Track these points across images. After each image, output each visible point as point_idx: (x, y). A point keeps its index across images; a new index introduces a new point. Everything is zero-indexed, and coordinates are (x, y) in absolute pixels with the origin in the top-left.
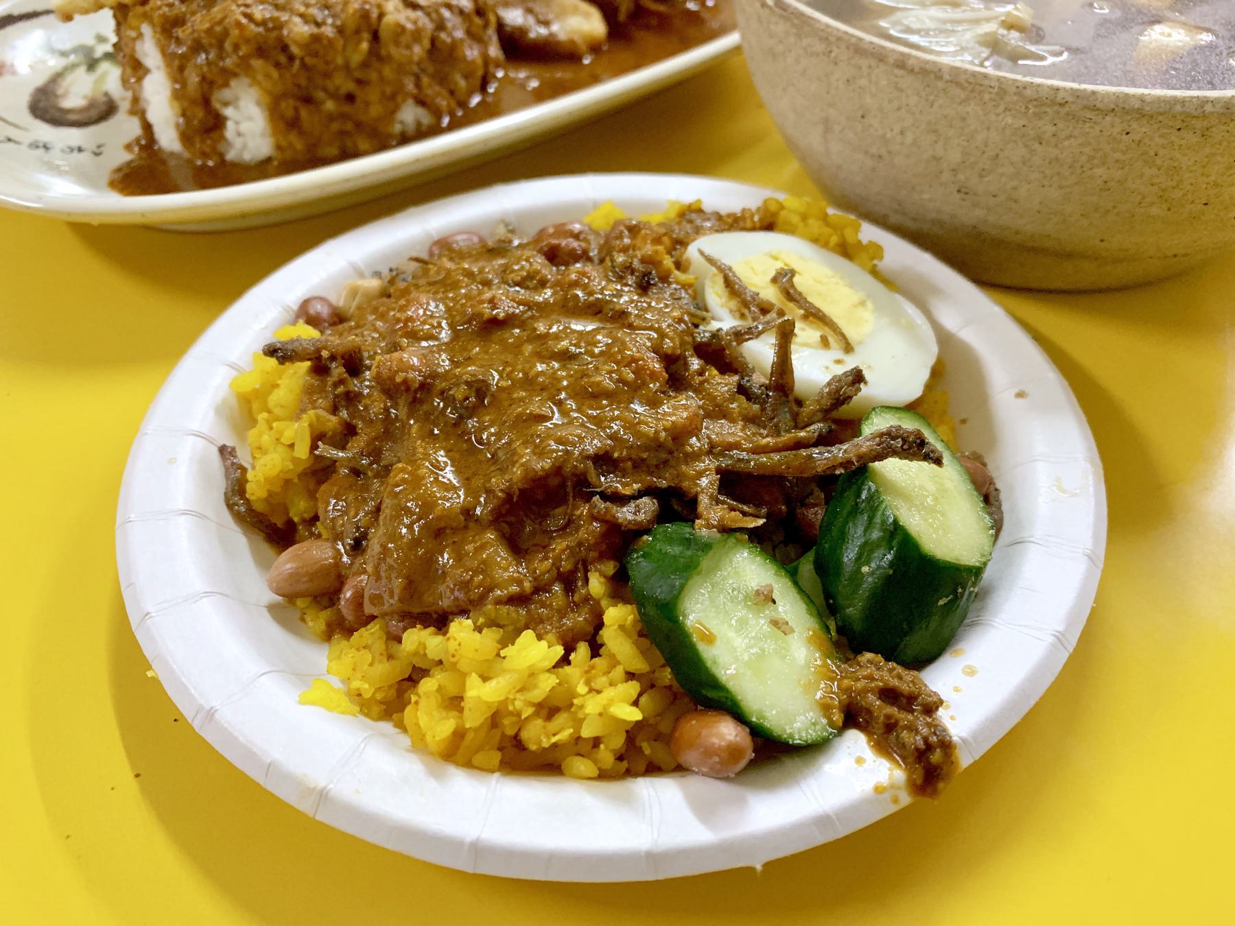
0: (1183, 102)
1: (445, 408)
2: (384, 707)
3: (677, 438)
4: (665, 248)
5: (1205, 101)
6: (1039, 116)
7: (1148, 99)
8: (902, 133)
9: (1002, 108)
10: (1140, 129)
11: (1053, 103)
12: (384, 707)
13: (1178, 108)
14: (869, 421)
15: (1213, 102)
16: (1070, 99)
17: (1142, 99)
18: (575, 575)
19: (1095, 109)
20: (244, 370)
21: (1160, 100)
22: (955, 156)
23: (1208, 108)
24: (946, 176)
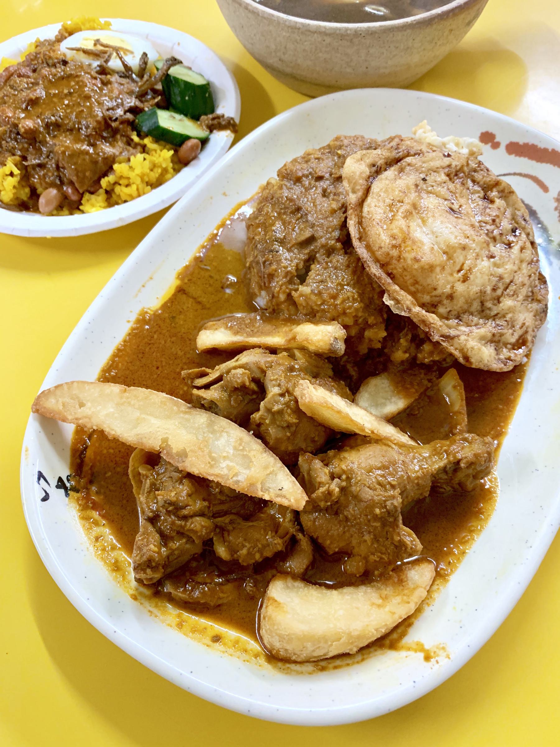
0: (340, 29)
1: (110, 374)
2: (81, 207)
3: (226, 195)
4: (10, 156)
5: (347, 29)
6: (294, 33)
7: (327, 28)
8: (255, 35)
9: (280, 29)
10: (328, 40)
11: (296, 28)
12: (81, 207)
13: (338, 32)
14: (363, 187)
15: (351, 29)
16: (301, 27)
17: (325, 27)
18: (344, 555)
19: (309, 31)
20: (459, 42)
21: (331, 28)
22: (273, 47)
23: (349, 32)
24: (273, 54)
